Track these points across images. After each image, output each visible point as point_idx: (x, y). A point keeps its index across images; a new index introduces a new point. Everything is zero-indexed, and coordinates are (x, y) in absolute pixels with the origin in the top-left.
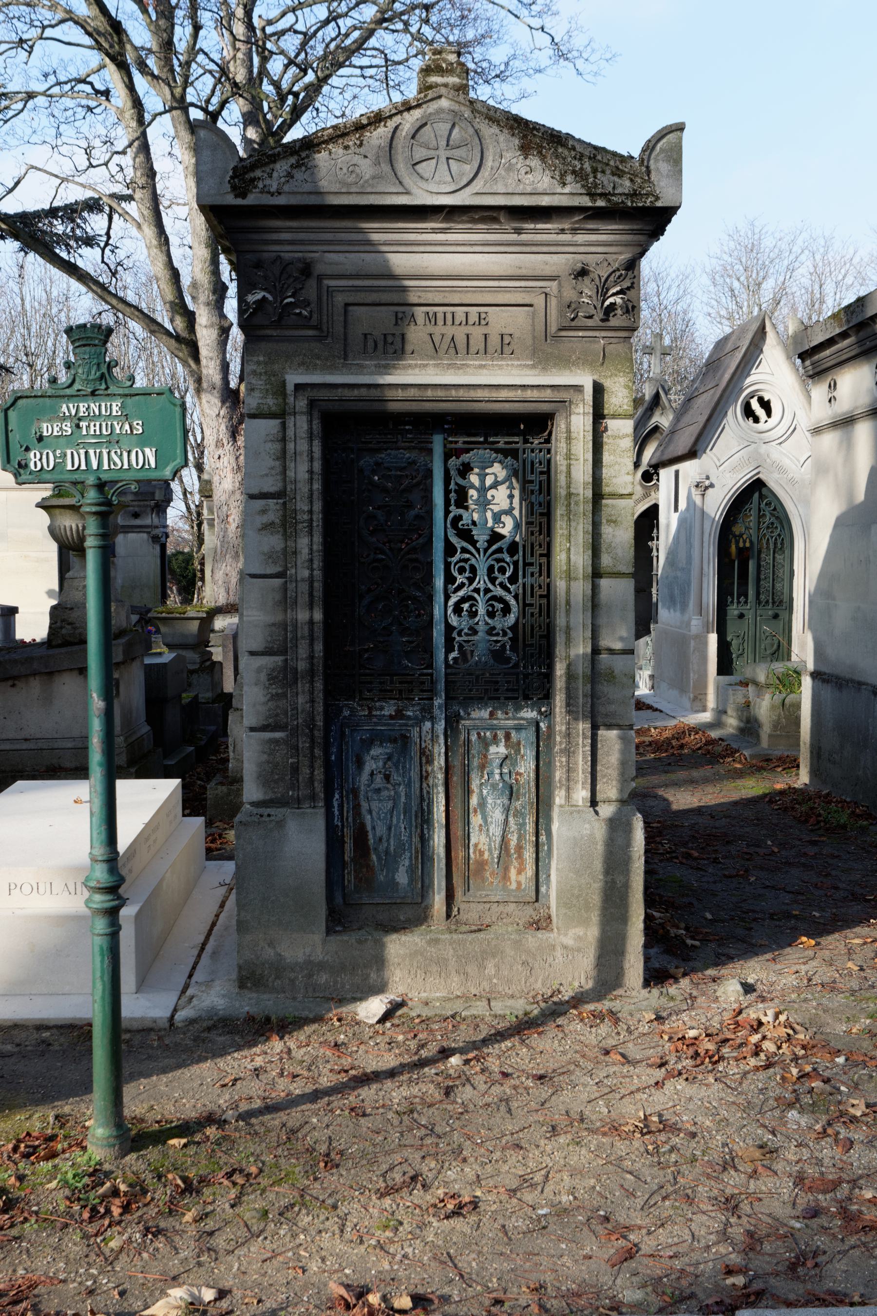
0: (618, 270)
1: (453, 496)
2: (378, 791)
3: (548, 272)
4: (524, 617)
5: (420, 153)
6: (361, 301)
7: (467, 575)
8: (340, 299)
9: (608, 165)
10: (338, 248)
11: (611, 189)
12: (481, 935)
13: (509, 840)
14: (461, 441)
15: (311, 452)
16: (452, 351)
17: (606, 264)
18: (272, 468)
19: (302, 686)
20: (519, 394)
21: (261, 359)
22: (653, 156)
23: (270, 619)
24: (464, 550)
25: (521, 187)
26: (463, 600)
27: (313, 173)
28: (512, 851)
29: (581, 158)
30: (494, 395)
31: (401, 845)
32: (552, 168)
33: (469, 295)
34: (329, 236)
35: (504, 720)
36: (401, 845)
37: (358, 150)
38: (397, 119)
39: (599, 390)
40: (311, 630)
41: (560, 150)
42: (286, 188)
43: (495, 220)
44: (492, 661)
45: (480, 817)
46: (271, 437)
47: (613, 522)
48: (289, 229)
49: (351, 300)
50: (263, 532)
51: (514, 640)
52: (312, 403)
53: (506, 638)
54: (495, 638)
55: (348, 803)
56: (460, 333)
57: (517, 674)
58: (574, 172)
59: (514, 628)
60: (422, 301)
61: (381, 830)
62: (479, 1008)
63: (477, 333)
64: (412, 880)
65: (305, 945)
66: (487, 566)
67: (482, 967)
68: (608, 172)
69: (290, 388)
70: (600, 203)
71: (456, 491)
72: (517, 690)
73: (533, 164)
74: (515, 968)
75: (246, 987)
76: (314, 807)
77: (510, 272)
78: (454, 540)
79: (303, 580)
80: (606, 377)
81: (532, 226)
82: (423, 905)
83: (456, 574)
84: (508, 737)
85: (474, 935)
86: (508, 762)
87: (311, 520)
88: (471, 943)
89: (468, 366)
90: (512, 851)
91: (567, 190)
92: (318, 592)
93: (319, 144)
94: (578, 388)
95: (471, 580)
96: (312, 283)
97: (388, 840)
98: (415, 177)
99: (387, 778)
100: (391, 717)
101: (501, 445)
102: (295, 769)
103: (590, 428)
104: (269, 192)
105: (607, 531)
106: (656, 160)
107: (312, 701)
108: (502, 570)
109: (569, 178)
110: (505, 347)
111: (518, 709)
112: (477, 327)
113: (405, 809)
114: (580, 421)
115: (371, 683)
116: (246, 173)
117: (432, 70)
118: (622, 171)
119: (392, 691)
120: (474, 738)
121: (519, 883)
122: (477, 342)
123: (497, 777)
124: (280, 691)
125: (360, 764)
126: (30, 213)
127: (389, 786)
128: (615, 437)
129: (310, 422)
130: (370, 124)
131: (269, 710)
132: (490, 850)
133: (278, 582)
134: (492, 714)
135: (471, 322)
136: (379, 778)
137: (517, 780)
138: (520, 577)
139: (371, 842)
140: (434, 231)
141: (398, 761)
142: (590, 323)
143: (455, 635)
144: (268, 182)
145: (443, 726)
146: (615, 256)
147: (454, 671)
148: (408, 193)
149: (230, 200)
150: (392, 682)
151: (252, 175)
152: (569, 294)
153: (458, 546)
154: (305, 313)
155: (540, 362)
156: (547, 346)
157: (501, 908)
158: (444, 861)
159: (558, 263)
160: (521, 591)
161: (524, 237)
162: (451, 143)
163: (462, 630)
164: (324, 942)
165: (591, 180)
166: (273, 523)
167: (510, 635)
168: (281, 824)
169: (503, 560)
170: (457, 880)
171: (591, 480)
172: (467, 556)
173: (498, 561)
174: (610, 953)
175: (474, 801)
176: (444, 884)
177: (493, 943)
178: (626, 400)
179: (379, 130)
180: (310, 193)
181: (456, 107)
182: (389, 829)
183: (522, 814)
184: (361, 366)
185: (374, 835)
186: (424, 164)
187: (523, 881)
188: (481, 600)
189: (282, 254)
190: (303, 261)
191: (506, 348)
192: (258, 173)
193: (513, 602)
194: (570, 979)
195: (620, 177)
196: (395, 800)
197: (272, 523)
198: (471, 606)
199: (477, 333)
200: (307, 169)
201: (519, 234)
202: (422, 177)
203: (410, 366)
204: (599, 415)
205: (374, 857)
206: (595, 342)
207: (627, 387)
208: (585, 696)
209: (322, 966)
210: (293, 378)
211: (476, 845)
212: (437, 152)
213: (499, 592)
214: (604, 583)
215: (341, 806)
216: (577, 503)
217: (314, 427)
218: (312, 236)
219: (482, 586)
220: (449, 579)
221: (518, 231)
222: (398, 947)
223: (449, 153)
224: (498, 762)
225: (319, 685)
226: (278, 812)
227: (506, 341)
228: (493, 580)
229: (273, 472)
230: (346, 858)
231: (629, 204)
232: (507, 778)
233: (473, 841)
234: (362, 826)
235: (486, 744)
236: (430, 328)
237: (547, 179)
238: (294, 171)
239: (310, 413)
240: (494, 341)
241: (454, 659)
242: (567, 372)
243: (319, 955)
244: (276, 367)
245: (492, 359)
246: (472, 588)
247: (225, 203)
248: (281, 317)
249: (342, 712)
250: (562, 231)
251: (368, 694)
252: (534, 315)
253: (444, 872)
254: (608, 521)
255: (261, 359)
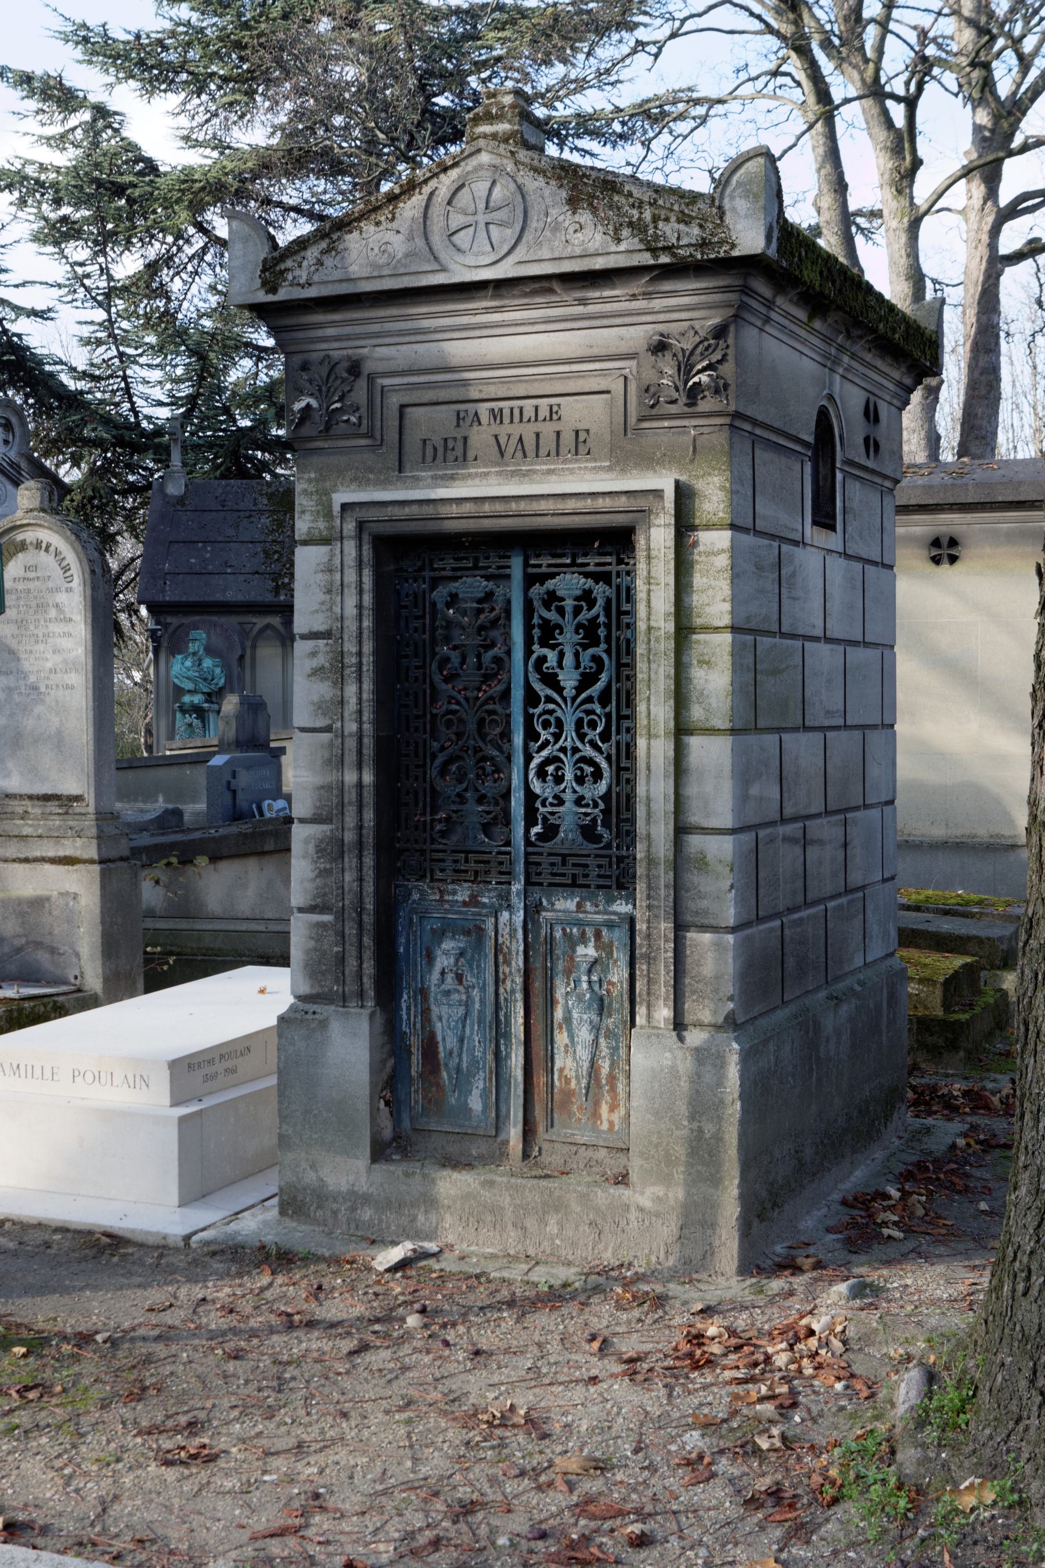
0: (706, 339)
1: (536, 632)
2: (448, 993)
3: (623, 348)
4: (618, 785)
5: (457, 220)
6: (417, 401)
7: (552, 730)
8: (394, 401)
9: (672, 210)
10: (387, 340)
11: (674, 241)
12: (544, 1183)
13: (600, 1067)
14: (544, 562)
15: (361, 582)
16: (519, 454)
17: (692, 333)
18: (322, 603)
19: (350, 861)
20: (589, 504)
21: (313, 475)
22: (728, 192)
23: (319, 780)
24: (549, 700)
25: (569, 249)
26: (548, 761)
27: (343, 258)
28: (604, 1081)
29: (640, 205)
30: (560, 506)
31: (474, 1062)
32: (605, 221)
33: (536, 385)
34: (375, 328)
35: (593, 914)
36: (474, 1062)
37: (389, 226)
38: (433, 184)
39: (684, 495)
40: (360, 795)
41: (616, 198)
42: (316, 278)
43: (551, 291)
44: (580, 839)
45: (566, 1034)
46: (322, 567)
47: (704, 663)
48: (333, 324)
49: (406, 400)
50: (313, 679)
51: (606, 812)
52: (361, 526)
53: (596, 811)
54: (583, 810)
55: (416, 1006)
56: (528, 431)
57: (610, 857)
58: (630, 224)
59: (606, 797)
60: (484, 396)
61: (451, 1042)
62: (516, 1273)
63: (548, 430)
64: (486, 1107)
65: (347, 1171)
66: (575, 718)
67: (543, 1222)
68: (673, 219)
69: (336, 508)
70: (664, 259)
71: (540, 626)
72: (610, 877)
73: (582, 220)
74: (581, 1229)
75: (287, 1215)
76: (362, 1007)
77: (579, 353)
78: (538, 686)
79: (350, 735)
80: (697, 477)
81: (597, 294)
82: (499, 1139)
83: (539, 729)
84: (598, 935)
85: (535, 1181)
86: (598, 967)
87: (360, 663)
88: (530, 1191)
89: (535, 472)
90: (604, 1081)
91: (622, 247)
92: (368, 750)
93: (349, 224)
94: (658, 493)
95: (557, 737)
96: (362, 383)
97: (460, 1055)
98: (452, 250)
99: (459, 978)
100: (465, 904)
101: (591, 568)
102: (341, 959)
103: (671, 543)
104: (299, 285)
105: (698, 674)
106: (732, 198)
107: (361, 879)
108: (593, 725)
109: (625, 232)
110: (580, 444)
111: (610, 901)
112: (548, 423)
113: (479, 1017)
114: (659, 537)
115: (443, 861)
116: (276, 265)
117: (481, 119)
118: (689, 216)
119: (466, 871)
120: (558, 934)
121: (611, 1123)
122: (548, 443)
123: (585, 986)
124: (328, 866)
125: (430, 958)
126: (998, 186)
127: (461, 988)
128: (709, 554)
129: (360, 548)
130: (402, 193)
131: (317, 888)
132: (577, 1077)
133: (326, 737)
134: (579, 905)
135: (541, 418)
136: (450, 978)
137: (608, 991)
138: (614, 733)
139: (442, 1055)
140: (488, 310)
141: (473, 957)
142: (673, 409)
143: (538, 804)
144: (297, 273)
145: (522, 918)
146: (703, 322)
147: (535, 850)
148: (444, 270)
149: (262, 297)
150: (467, 861)
151: (282, 266)
152: (649, 376)
153: (542, 694)
154: (353, 419)
155: (618, 462)
156: (627, 445)
157: (590, 1153)
158: (521, 1087)
159: (636, 336)
160: (614, 751)
161: (591, 309)
162: (492, 204)
163: (546, 799)
164: (369, 1170)
165: (651, 232)
166: (323, 668)
167: (602, 806)
168: (324, 1024)
169: (593, 712)
170: (539, 1112)
171: (672, 610)
172: (552, 706)
173: (588, 712)
174: (696, 1220)
175: (559, 1014)
176: (520, 1115)
177: (557, 1193)
178: (722, 506)
179: (414, 199)
180: (341, 281)
181: (497, 161)
182: (461, 1041)
183: (615, 1035)
184: (417, 479)
185: (445, 1047)
186: (462, 233)
187: (616, 1121)
188: (568, 762)
189: (331, 353)
190: (349, 358)
191: (581, 447)
192: (289, 263)
193: (604, 765)
194: (646, 1251)
195: (686, 223)
196: (468, 1004)
197: (322, 668)
198: (558, 769)
199: (548, 430)
200: (338, 253)
201: (585, 304)
202: (459, 250)
203: (470, 475)
204: (684, 526)
205: (445, 1074)
206: (684, 433)
207: (722, 488)
208: (666, 886)
209: (366, 1199)
210: (340, 497)
211: (561, 1070)
212: (476, 218)
213: (588, 751)
214: (694, 742)
215: (408, 1008)
216: (657, 640)
217: (365, 553)
218: (358, 329)
219: (569, 744)
220: (531, 734)
221: (583, 302)
222: (451, 1185)
223: (488, 217)
224: (584, 967)
225: (369, 861)
226: (326, 1010)
227: (581, 439)
228: (582, 737)
229: (324, 608)
230: (413, 1073)
231: (699, 257)
232: (596, 988)
233: (558, 1065)
234: (432, 1036)
235: (572, 943)
236: (495, 429)
237: (599, 237)
238: (324, 257)
239: (359, 538)
240: (568, 438)
241: (537, 834)
242: (650, 474)
243: (363, 1186)
244: (328, 484)
245: (564, 462)
246: (557, 746)
247: (256, 301)
248: (328, 427)
249: (410, 894)
250: (634, 297)
251: (439, 875)
252: (611, 405)
253: (521, 1101)
254: (699, 662)
255: (313, 475)
